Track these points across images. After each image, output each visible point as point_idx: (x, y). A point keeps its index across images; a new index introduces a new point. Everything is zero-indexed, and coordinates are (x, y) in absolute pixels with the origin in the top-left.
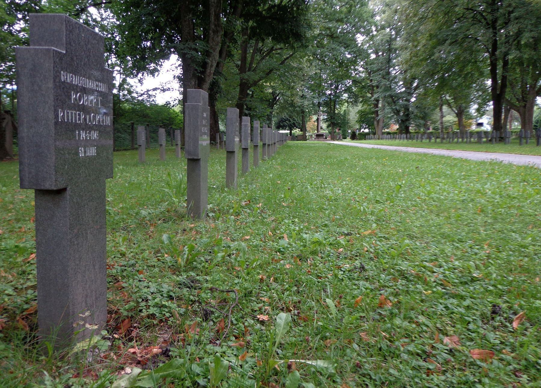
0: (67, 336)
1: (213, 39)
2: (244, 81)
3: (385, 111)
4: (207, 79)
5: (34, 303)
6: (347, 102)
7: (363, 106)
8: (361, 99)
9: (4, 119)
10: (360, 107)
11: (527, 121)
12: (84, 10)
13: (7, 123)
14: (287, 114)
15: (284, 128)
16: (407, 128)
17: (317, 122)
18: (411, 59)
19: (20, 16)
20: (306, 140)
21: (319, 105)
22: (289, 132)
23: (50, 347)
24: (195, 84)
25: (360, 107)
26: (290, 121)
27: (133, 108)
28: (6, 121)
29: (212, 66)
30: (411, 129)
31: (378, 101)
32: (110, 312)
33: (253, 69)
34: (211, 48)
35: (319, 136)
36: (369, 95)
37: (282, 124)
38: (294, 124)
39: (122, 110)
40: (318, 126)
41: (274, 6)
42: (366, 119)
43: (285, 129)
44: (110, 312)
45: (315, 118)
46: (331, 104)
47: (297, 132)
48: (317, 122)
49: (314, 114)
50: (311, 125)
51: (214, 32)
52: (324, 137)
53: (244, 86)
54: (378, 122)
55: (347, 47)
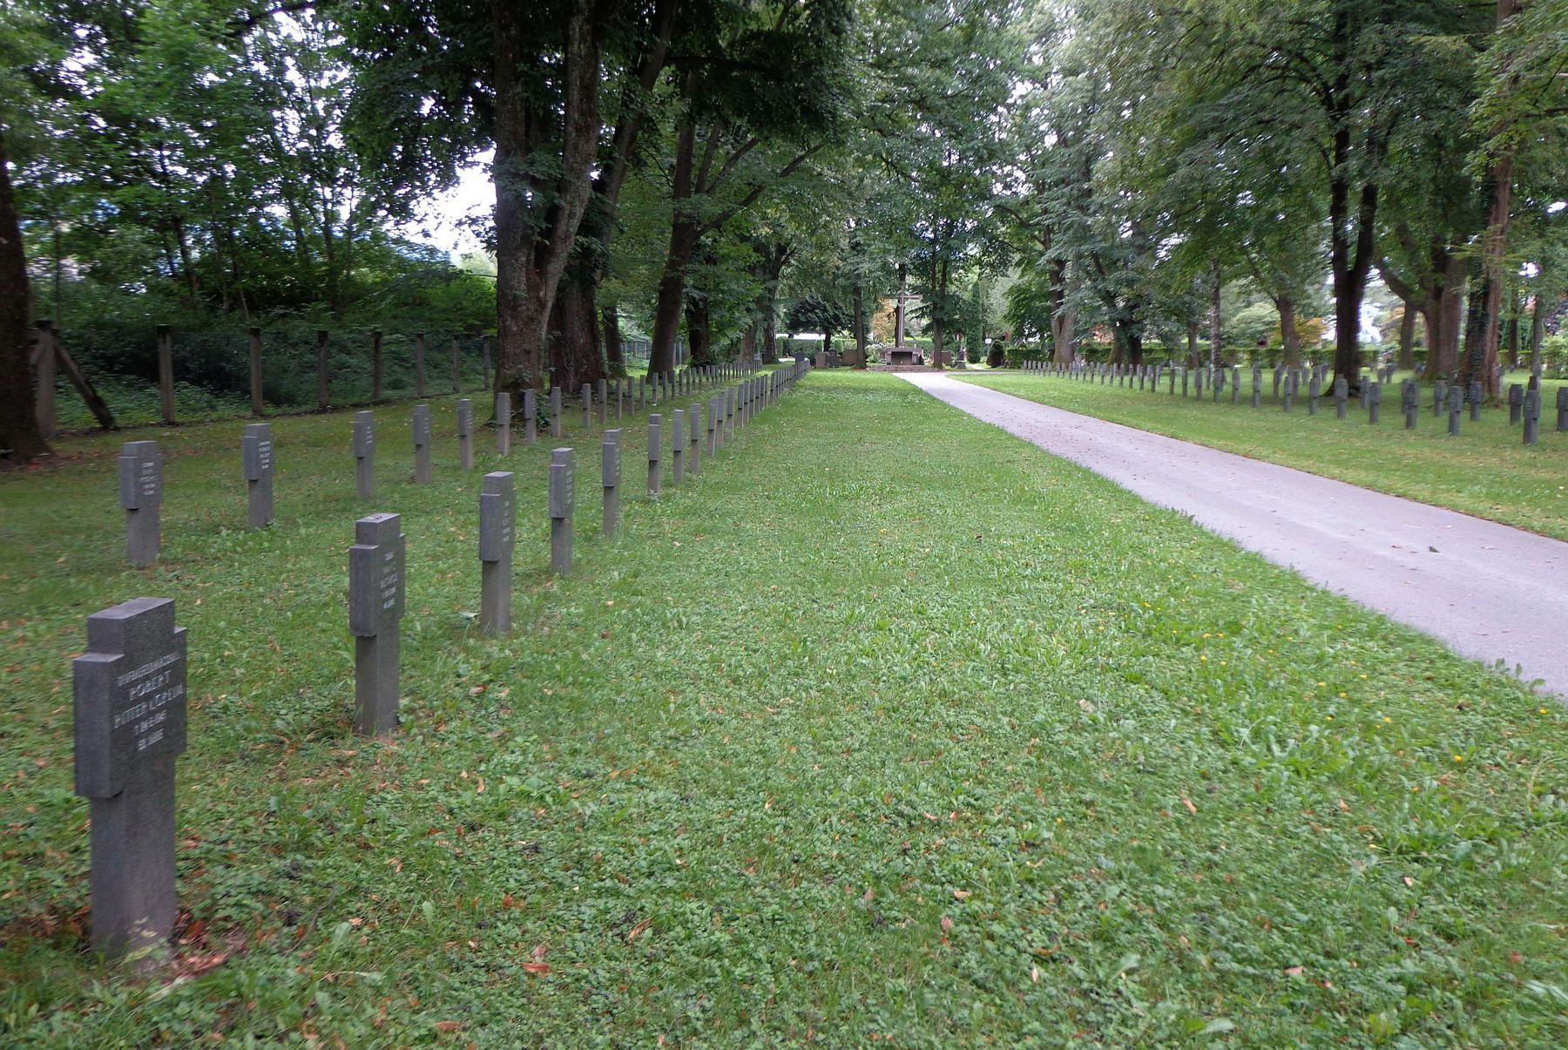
0: (121, 943)
1: (576, 147)
2: (681, 220)
3: (1080, 294)
4: (559, 248)
5: (88, 899)
6: (979, 262)
7: (1022, 276)
8: (1017, 257)
9: (35, 342)
10: (1014, 277)
11: (1443, 336)
12: (260, 17)
13: (42, 355)
14: (818, 290)
15: (808, 326)
16: (1135, 343)
17: (901, 313)
18: (1123, 172)
19: (82, 33)
20: (863, 367)
21: (903, 270)
22: (823, 337)
23: (101, 957)
24: (528, 261)
25: (1014, 277)
26: (825, 310)
27: (384, 282)
28: (39, 348)
29: (571, 216)
30: (1149, 341)
31: (1061, 263)
32: (182, 911)
33: (707, 186)
34: (572, 169)
35: (900, 358)
36: (1039, 247)
37: (802, 319)
38: (836, 317)
39: (355, 285)
40: (897, 329)
41: (755, 35)
42: (1027, 309)
43: (813, 331)
44: (182, 911)
45: (891, 304)
46: (934, 269)
47: (844, 339)
48: (901, 313)
49: (888, 297)
50: (879, 325)
51: (578, 130)
52: (915, 359)
53: (685, 237)
54: (1061, 320)
55: (956, 135)
